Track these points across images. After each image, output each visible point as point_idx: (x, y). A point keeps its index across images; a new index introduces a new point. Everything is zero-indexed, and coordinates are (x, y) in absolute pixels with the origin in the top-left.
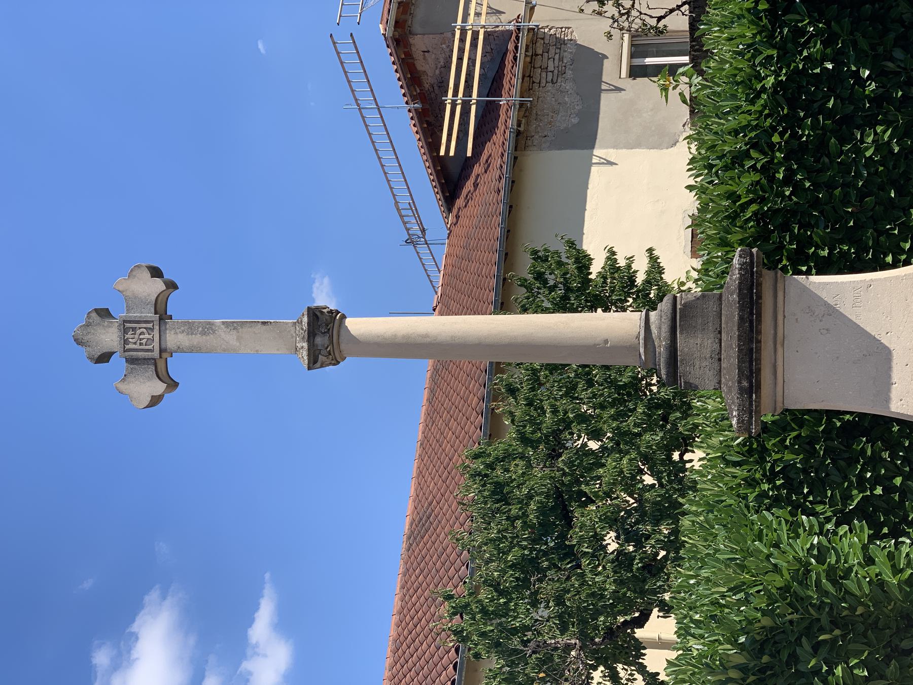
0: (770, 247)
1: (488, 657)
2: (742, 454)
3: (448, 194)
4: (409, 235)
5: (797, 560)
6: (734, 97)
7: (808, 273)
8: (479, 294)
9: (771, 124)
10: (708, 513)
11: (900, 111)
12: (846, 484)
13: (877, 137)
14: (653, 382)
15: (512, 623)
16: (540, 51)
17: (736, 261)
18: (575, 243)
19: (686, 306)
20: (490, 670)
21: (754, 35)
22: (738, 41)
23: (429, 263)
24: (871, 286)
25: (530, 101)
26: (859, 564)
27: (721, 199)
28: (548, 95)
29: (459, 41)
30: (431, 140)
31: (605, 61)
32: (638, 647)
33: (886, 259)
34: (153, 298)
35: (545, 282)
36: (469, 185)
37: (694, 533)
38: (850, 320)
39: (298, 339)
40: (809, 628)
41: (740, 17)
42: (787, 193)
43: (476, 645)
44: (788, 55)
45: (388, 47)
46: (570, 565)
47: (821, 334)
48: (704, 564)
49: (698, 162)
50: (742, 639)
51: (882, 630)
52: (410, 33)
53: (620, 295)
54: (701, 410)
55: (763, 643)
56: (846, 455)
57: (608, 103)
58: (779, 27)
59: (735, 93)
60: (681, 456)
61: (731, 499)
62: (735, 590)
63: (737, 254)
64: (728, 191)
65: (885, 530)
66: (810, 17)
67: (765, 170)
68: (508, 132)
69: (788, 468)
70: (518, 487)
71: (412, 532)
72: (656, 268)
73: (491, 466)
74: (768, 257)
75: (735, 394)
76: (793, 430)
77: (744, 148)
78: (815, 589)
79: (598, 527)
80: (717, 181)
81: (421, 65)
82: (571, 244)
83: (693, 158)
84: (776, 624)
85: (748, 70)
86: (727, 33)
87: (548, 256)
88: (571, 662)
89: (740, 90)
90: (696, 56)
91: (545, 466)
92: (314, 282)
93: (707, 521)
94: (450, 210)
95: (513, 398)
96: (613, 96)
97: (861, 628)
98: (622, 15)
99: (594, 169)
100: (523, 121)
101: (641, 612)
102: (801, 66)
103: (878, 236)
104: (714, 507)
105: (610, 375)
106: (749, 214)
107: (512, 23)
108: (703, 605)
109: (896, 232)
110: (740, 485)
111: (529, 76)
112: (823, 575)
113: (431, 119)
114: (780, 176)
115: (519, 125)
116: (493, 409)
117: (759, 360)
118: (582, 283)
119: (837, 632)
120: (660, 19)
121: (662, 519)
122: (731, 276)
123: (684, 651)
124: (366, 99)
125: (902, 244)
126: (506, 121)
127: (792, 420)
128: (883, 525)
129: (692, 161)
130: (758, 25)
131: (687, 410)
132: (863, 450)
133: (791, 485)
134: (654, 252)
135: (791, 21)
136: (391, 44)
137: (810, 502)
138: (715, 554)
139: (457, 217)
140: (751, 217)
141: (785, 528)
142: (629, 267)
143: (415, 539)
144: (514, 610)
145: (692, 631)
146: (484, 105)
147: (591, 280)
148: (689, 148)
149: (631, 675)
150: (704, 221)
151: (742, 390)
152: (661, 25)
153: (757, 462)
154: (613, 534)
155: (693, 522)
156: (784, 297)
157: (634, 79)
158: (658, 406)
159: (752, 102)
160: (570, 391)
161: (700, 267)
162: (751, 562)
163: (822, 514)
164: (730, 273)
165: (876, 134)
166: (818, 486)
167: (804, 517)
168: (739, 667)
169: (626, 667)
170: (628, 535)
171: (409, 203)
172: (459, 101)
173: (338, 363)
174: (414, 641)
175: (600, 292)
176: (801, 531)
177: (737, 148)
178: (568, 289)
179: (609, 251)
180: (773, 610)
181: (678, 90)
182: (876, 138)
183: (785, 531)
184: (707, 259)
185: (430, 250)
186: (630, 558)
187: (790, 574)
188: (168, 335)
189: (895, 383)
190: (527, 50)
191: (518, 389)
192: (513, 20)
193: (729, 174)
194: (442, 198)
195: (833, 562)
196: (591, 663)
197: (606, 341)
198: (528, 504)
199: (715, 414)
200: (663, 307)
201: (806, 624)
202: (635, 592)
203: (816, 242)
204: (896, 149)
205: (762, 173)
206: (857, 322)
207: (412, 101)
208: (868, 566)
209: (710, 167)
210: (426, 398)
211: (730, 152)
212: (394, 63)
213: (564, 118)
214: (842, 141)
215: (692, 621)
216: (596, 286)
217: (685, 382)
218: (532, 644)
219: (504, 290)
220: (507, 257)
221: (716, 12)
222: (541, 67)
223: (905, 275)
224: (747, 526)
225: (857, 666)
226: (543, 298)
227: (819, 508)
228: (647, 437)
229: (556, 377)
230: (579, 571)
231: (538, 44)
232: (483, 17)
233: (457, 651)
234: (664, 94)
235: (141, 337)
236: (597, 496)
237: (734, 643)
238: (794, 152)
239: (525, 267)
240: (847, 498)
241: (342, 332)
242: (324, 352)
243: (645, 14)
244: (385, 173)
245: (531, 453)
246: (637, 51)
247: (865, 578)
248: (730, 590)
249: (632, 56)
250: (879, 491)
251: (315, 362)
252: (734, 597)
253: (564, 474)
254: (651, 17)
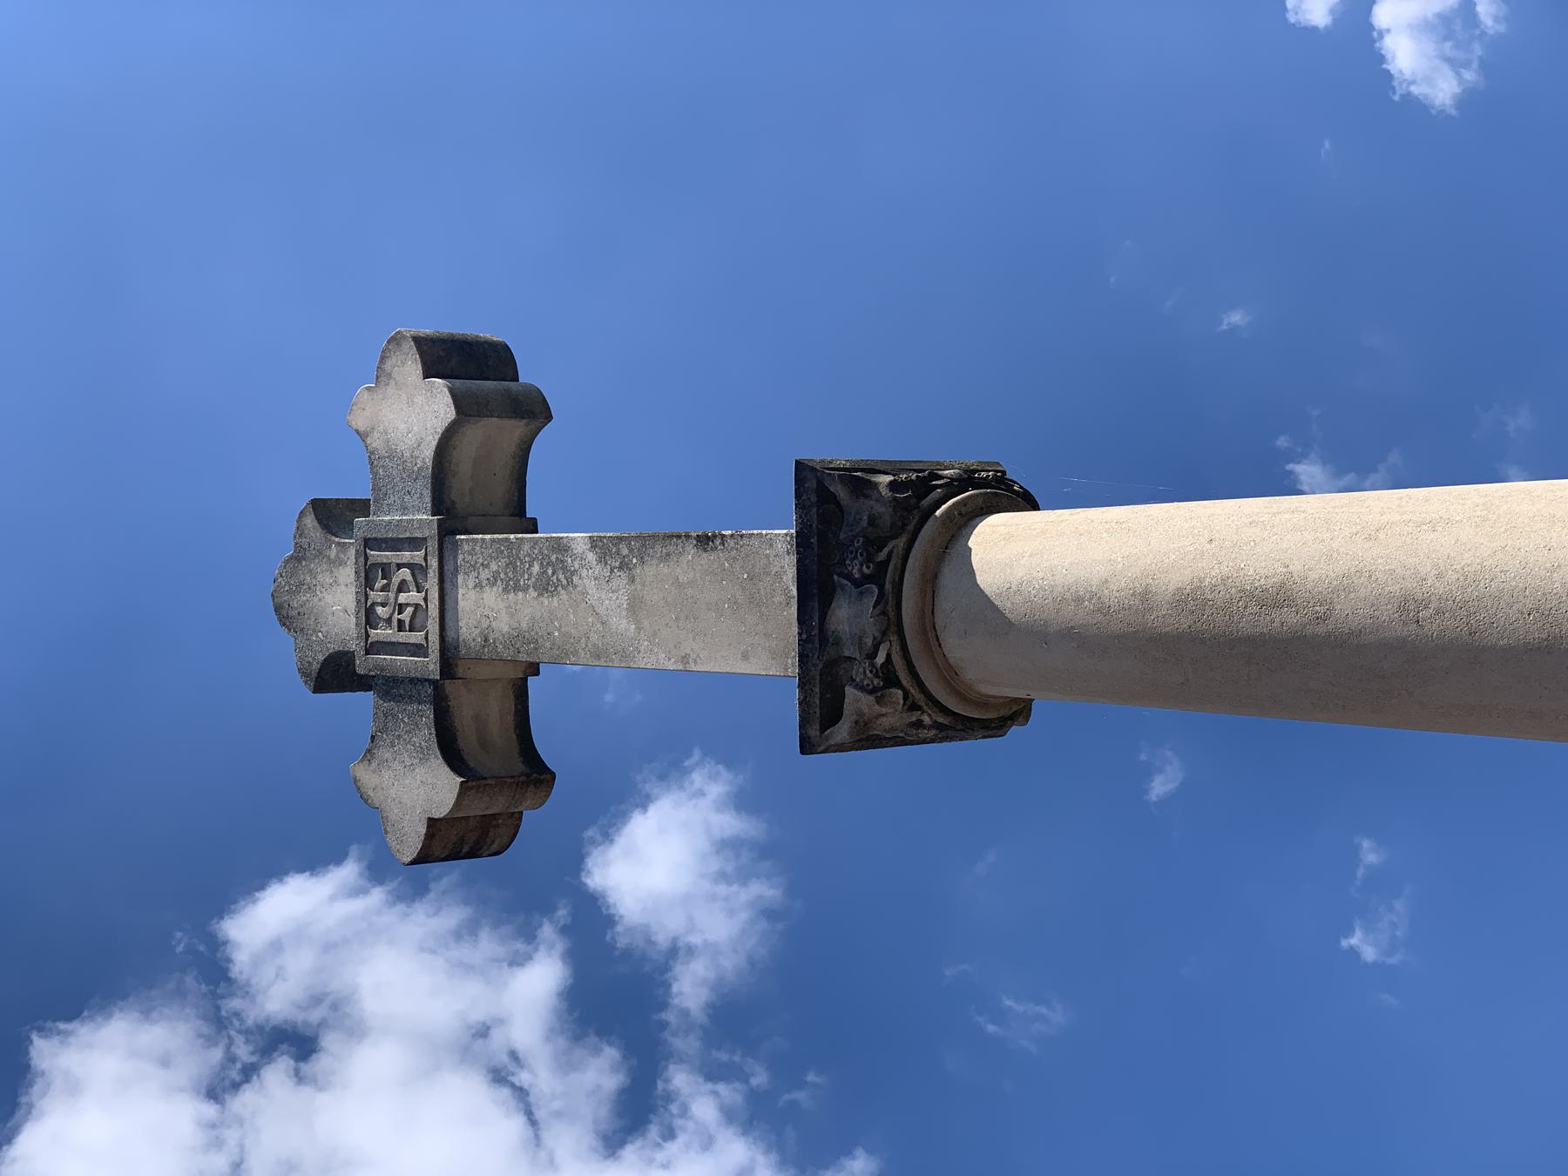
34: (428, 453)
188: (461, 591)
235: (403, 598)
241: (948, 577)
242: (861, 672)
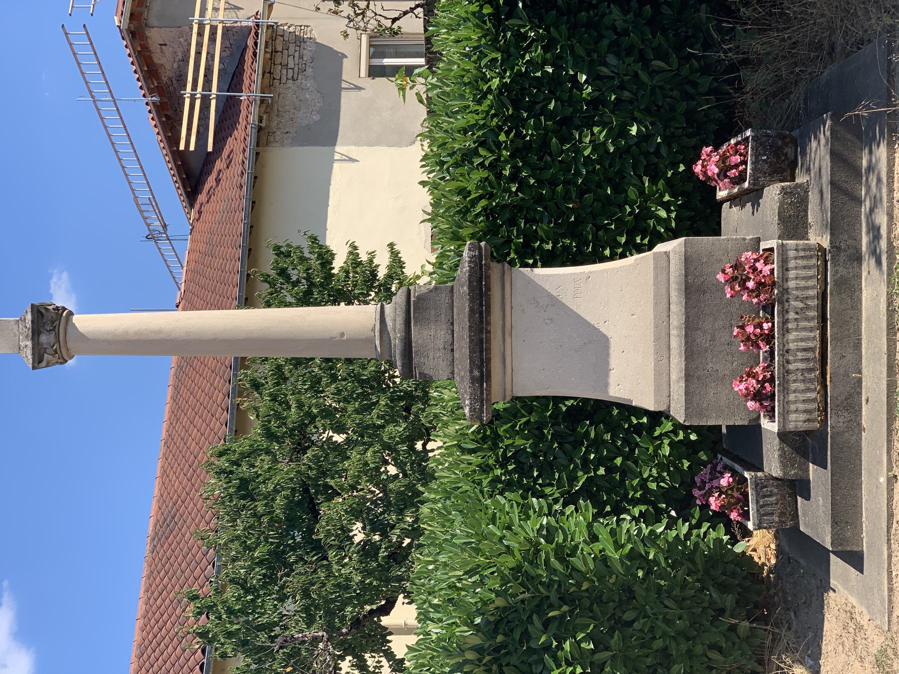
0: (499, 241)
1: (235, 656)
2: (477, 442)
3: (190, 190)
4: (149, 230)
5: (527, 540)
6: (462, 97)
7: (535, 265)
8: (223, 290)
9: (497, 123)
10: (445, 500)
11: (614, 114)
12: (572, 466)
13: (594, 137)
14: (396, 374)
15: (259, 619)
16: (279, 48)
17: (465, 254)
18: (318, 238)
19: (420, 298)
20: (237, 668)
21: (480, 39)
22: (465, 43)
23: (171, 259)
25: (271, 97)
26: (585, 541)
27: (453, 195)
28: (289, 93)
29: (198, 35)
30: (170, 134)
31: (345, 60)
32: (384, 634)
33: (605, 252)
35: (288, 278)
36: (211, 180)
37: (433, 519)
39: (21, 337)
40: (538, 606)
41: (466, 20)
42: (514, 189)
43: (223, 644)
44: (511, 58)
45: (123, 38)
46: (315, 558)
48: (442, 549)
49: (430, 158)
50: (478, 620)
51: (606, 603)
52: (146, 25)
53: (362, 289)
54: (439, 400)
55: (497, 623)
56: (572, 439)
57: (348, 102)
58: (502, 31)
59: (463, 93)
60: (424, 445)
61: (467, 485)
62: (470, 573)
63: (466, 248)
64: (459, 187)
65: (608, 508)
66: (531, 22)
67: (492, 167)
68: (249, 127)
69: (519, 452)
70: (264, 482)
71: (157, 534)
72: (397, 262)
73: (237, 463)
74: (497, 250)
75: (467, 383)
76: (524, 416)
77: (473, 146)
78: (544, 567)
79: (344, 520)
80: (448, 178)
81: (158, 59)
82: (314, 239)
83: (426, 155)
84: (509, 603)
85: (474, 72)
86: (454, 35)
87: (290, 251)
88: (318, 654)
89: (467, 91)
90: (431, 58)
91: (291, 460)
92: (51, 278)
93: (444, 508)
94: (192, 206)
95: (258, 393)
96: (353, 94)
97: (586, 603)
98: (357, 15)
99: (336, 166)
100: (265, 117)
101: (387, 600)
102: (523, 70)
103: (597, 231)
104: (451, 493)
105: (353, 370)
106: (478, 209)
107: (251, 20)
108: (441, 589)
109: (613, 227)
110: (475, 471)
111: (270, 72)
112: (552, 554)
113: (170, 113)
114: (507, 173)
115: (260, 121)
116: (238, 405)
117: (488, 350)
118: (325, 278)
119: (565, 608)
120: (394, 20)
121: (406, 508)
122: (461, 269)
123: (424, 635)
124: (101, 91)
125: (619, 238)
126: (247, 117)
127: (522, 407)
128: (605, 504)
129: (425, 157)
130: (482, 29)
131: (425, 399)
132: (587, 433)
133: (522, 469)
134: (395, 247)
135: (514, 25)
136: (126, 36)
137: (540, 485)
138: (452, 539)
139: (200, 212)
140: (481, 212)
141: (516, 511)
142: (371, 261)
143: (159, 540)
144: (262, 607)
145: (432, 615)
146: (225, 100)
147: (333, 275)
148: (422, 145)
149: (379, 662)
150: (437, 215)
151: (473, 380)
152: (395, 26)
153: (491, 449)
154: (359, 525)
155: (432, 509)
157: (373, 79)
158: (400, 398)
159: (479, 102)
160: (315, 385)
161: (434, 261)
162: (485, 545)
163: (551, 495)
164: (461, 266)
165: (593, 134)
166: (547, 470)
167: (534, 500)
168: (474, 649)
169: (373, 654)
170: (375, 525)
171: (149, 198)
172: (198, 96)
173: (66, 361)
174: (159, 645)
175: (343, 286)
176: (531, 512)
177: (465, 146)
178: (312, 285)
179: (350, 246)
180: (507, 590)
181: (415, 91)
182: (593, 138)
183: (516, 514)
184: (441, 253)
185: (172, 246)
186: (376, 548)
187: (521, 554)
190: (266, 47)
191: (263, 385)
192: (252, 17)
193: (459, 170)
194: (184, 194)
195: (561, 541)
196: (338, 653)
197: (342, 334)
198: (273, 500)
199: (451, 403)
200: (398, 300)
201: (536, 602)
202: (381, 580)
203: (541, 237)
204: (612, 149)
205: (490, 171)
207: (150, 94)
208: (593, 543)
209: (442, 164)
210: (169, 396)
211: (459, 149)
212: (129, 55)
213: (305, 115)
214: (563, 141)
215: (431, 605)
216: (338, 280)
217: (420, 373)
218: (279, 640)
219: (248, 286)
220: (251, 253)
221: (444, 14)
222: (281, 64)
223: (620, 267)
224: (481, 510)
225: (583, 640)
226: (286, 294)
227: (548, 490)
228: (390, 428)
229: (301, 370)
230: (325, 562)
231: (278, 41)
232: (221, 12)
233: (203, 651)
234: (401, 93)
236: (343, 489)
237: (470, 624)
238: (520, 151)
239: (268, 263)
240: (573, 479)
241: (69, 329)
243: (380, 15)
244: (123, 167)
245: (276, 448)
246: (377, 51)
247: (590, 554)
248: (466, 573)
249: (371, 56)
250: (602, 471)
251: (40, 361)
252: (469, 580)
253: (310, 468)
254: (386, 18)
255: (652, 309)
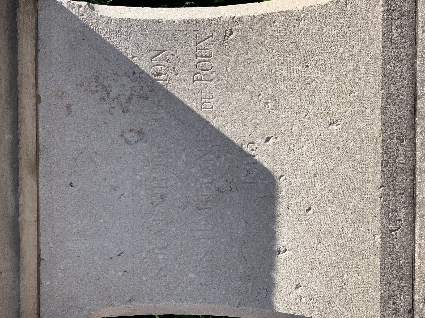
24: (231, 33)
38: (189, 111)
47: (126, 141)
156: (37, 51)
189: (285, 251)
206: (205, 114)
223: (304, 10)
255: (378, 111)
